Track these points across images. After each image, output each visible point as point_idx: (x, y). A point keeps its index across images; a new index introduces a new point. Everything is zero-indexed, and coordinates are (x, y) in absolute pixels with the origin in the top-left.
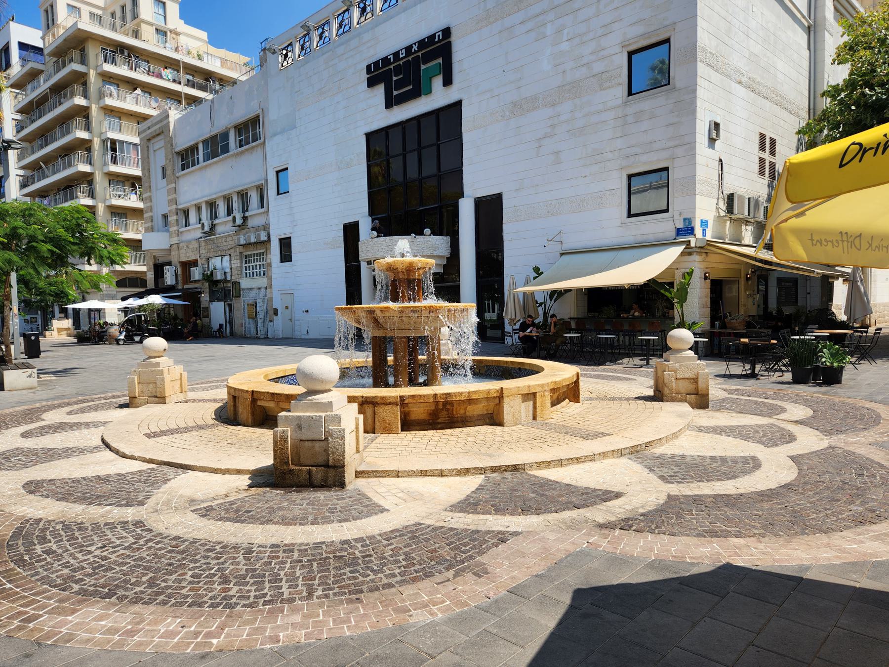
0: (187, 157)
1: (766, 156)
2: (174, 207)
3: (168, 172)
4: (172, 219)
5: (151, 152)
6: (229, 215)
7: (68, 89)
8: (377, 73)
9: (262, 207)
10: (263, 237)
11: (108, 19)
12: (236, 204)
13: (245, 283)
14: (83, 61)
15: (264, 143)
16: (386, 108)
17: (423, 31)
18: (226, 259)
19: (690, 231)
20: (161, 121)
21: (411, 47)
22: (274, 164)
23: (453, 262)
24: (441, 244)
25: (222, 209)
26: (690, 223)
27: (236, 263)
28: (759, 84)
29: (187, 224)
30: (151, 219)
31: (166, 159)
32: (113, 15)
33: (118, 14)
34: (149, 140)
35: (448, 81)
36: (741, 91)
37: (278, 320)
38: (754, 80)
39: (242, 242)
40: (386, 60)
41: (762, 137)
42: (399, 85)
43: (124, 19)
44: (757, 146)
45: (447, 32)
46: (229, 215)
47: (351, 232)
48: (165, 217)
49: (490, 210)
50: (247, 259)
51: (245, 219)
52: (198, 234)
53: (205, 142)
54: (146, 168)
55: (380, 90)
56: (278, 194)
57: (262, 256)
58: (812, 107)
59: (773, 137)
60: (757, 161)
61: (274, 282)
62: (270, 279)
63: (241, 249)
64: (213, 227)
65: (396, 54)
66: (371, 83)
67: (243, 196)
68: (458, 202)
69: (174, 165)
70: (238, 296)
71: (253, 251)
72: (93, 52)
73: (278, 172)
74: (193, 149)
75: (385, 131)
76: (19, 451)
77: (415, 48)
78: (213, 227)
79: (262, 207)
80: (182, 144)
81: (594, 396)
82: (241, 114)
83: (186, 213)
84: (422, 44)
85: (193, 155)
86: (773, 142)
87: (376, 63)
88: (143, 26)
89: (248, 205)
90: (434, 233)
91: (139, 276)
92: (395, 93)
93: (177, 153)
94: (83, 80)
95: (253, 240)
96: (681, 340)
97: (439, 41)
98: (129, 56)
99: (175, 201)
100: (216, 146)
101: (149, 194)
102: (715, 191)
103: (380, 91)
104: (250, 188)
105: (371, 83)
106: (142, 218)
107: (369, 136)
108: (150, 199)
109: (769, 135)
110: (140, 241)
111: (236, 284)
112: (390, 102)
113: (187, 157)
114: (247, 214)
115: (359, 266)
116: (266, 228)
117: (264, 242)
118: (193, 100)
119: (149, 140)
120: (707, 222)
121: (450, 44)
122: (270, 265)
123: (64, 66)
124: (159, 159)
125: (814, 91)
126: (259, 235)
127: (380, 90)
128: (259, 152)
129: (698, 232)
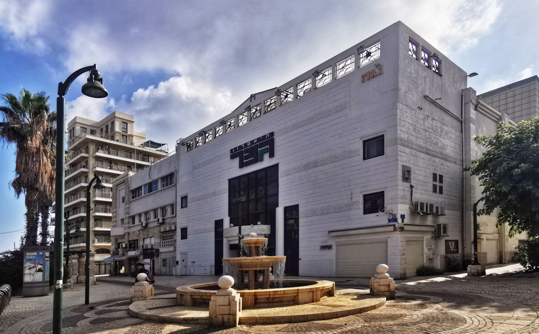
0: (136, 193)
1: (438, 184)
2: (128, 215)
3: (126, 200)
4: (126, 221)
5: (118, 191)
6: (155, 218)
7: (79, 165)
8: (235, 153)
9: (173, 214)
10: (173, 228)
11: (98, 131)
12: (159, 212)
13: (162, 250)
14: (87, 152)
15: (176, 185)
16: (240, 168)
17: (260, 134)
18: (153, 239)
19: (395, 220)
20: (124, 177)
21: (253, 141)
22: (181, 194)
23: (272, 237)
24: (265, 229)
25: (152, 214)
26: (395, 216)
27: (158, 241)
28: (432, 151)
29: (134, 223)
30: (116, 221)
31: (125, 194)
32: (102, 130)
33: (104, 129)
34: (117, 186)
35: (272, 155)
36: (423, 155)
37: (179, 267)
38: (429, 150)
39: (162, 230)
40: (240, 147)
41: (435, 175)
42: (247, 158)
43: (107, 131)
44: (431, 179)
45: (272, 134)
46: (155, 218)
47: (219, 224)
48: (122, 220)
49: (292, 212)
50: (164, 238)
51: (163, 219)
52: (140, 228)
53: (145, 185)
54: (114, 198)
55: (237, 160)
56: (182, 208)
57: (171, 237)
58: (464, 158)
59: (441, 174)
60: (432, 186)
61: (177, 249)
62: (175, 248)
63: (161, 234)
64: (147, 224)
65: (246, 145)
66: (232, 157)
67: (163, 209)
68: (275, 210)
69: (129, 197)
70: (158, 256)
71: (167, 236)
72: (92, 148)
73: (182, 198)
74: (139, 188)
75: (239, 178)
76: (104, 310)
77: (255, 141)
78: (147, 224)
79: (173, 214)
80: (134, 186)
81: (83, 278)
82: (165, 172)
83: (133, 218)
84: (259, 139)
85: (139, 192)
86: (441, 177)
87: (235, 149)
88: (116, 134)
89: (165, 214)
90: (262, 224)
91: (106, 248)
92: (245, 161)
93: (131, 191)
94: (86, 160)
95: (168, 229)
96: (229, 281)
97: (268, 138)
98: (109, 148)
99: (128, 213)
100: (151, 187)
101: (115, 210)
102: (408, 201)
103: (237, 161)
104: (168, 206)
105: (232, 157)
106: (111, 221)
107: (230, 181)
108: (116, 212)
109: (438, 173)
110: (110, 231)
111: (157, 250)
112: (242, 165)
113: (136, 193)
114: (165, 218)
115: (223, 240)
116: (175, 224)
117: (173, 230)
118: (140, 166)
119: (117, 186)
120: (404, 215)
121: (273, 139)
122: (175, 241)
123: (78, 155)
124: (122, 193)
125: (115, 319)
126: (171, 227)
127: (237, 160)
128: (174, 188)
129: (400, 220)
